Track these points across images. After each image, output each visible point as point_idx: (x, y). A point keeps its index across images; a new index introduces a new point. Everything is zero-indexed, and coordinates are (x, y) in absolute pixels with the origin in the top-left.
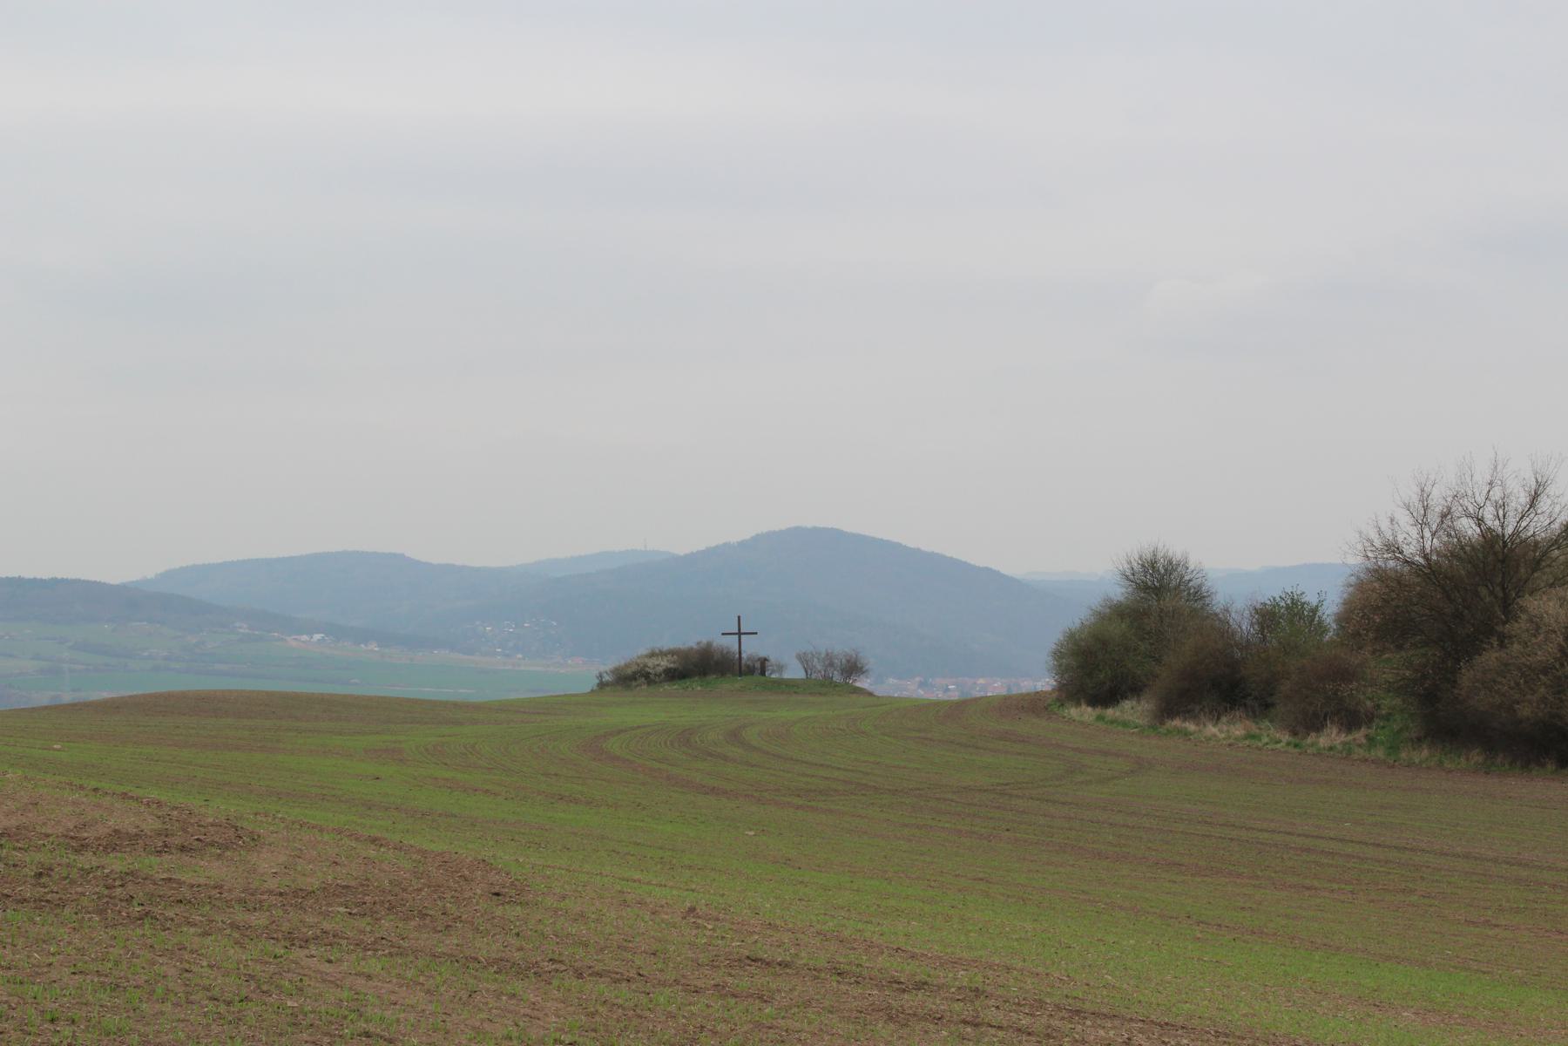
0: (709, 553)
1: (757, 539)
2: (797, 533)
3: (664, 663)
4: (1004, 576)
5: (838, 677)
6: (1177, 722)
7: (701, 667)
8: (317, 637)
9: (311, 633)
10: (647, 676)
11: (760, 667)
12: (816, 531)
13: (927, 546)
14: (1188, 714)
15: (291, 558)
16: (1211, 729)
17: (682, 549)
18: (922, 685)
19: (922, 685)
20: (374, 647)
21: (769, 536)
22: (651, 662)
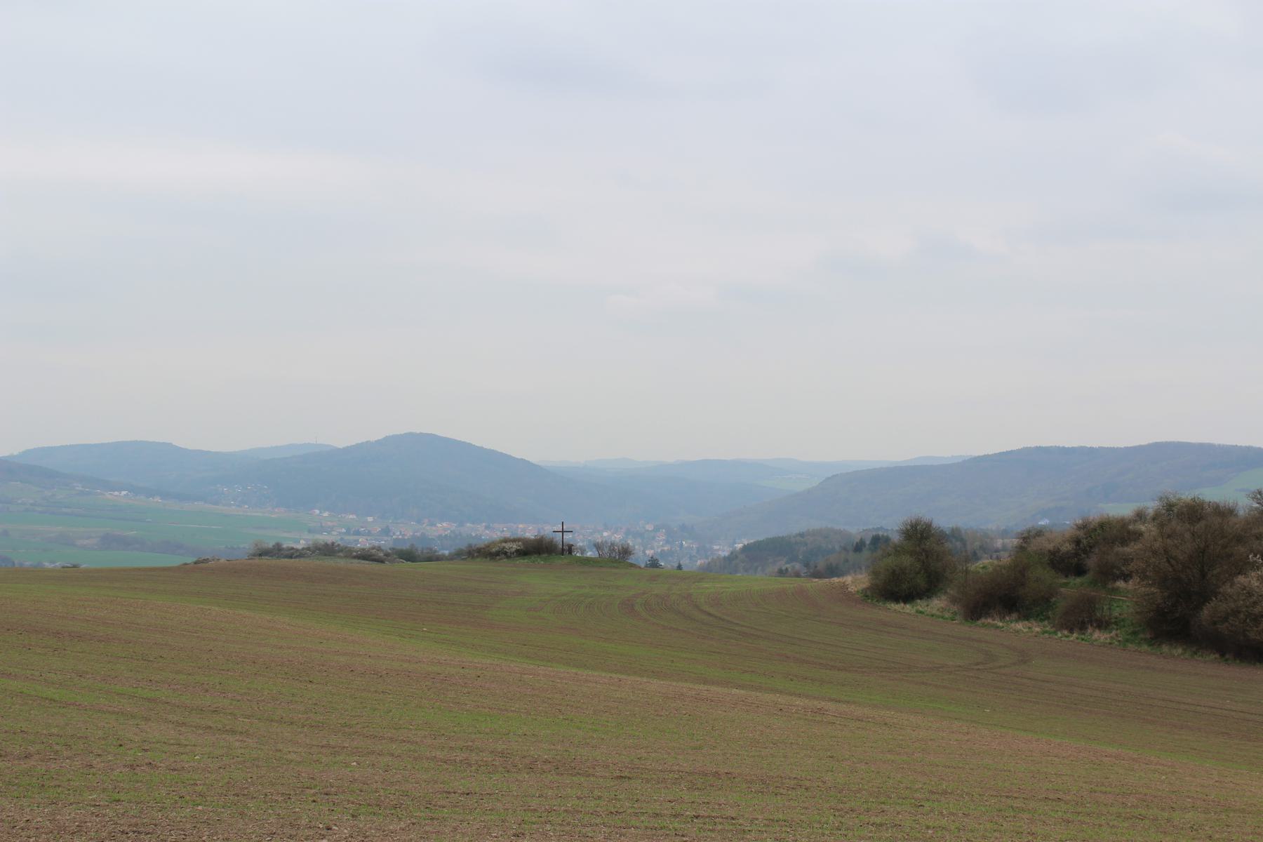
0: (358, 447)
1: (386, 438)
2: (411, 435)
3: (515, 546)
4: (514, 459)
5: (620, 557)
6: (983, 620)
7: (538, 550)
8: (124, 493)
9: (120, 491)
10: (505, 553)
11: (570, 549)
12: (492, 453)
13: (488, 445)
14: (987, 615)
15: (102, 445)
16: (1019, 626)
17: (341, 443)
18: (487, 527)
19: (487, 527)
20: (158, 499)
21: (394, 437)
22: (507, 546)
